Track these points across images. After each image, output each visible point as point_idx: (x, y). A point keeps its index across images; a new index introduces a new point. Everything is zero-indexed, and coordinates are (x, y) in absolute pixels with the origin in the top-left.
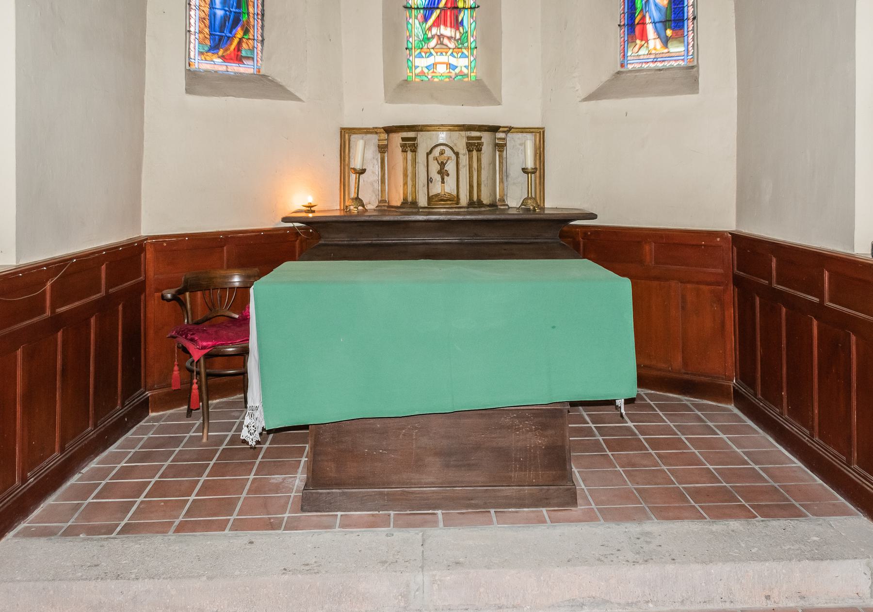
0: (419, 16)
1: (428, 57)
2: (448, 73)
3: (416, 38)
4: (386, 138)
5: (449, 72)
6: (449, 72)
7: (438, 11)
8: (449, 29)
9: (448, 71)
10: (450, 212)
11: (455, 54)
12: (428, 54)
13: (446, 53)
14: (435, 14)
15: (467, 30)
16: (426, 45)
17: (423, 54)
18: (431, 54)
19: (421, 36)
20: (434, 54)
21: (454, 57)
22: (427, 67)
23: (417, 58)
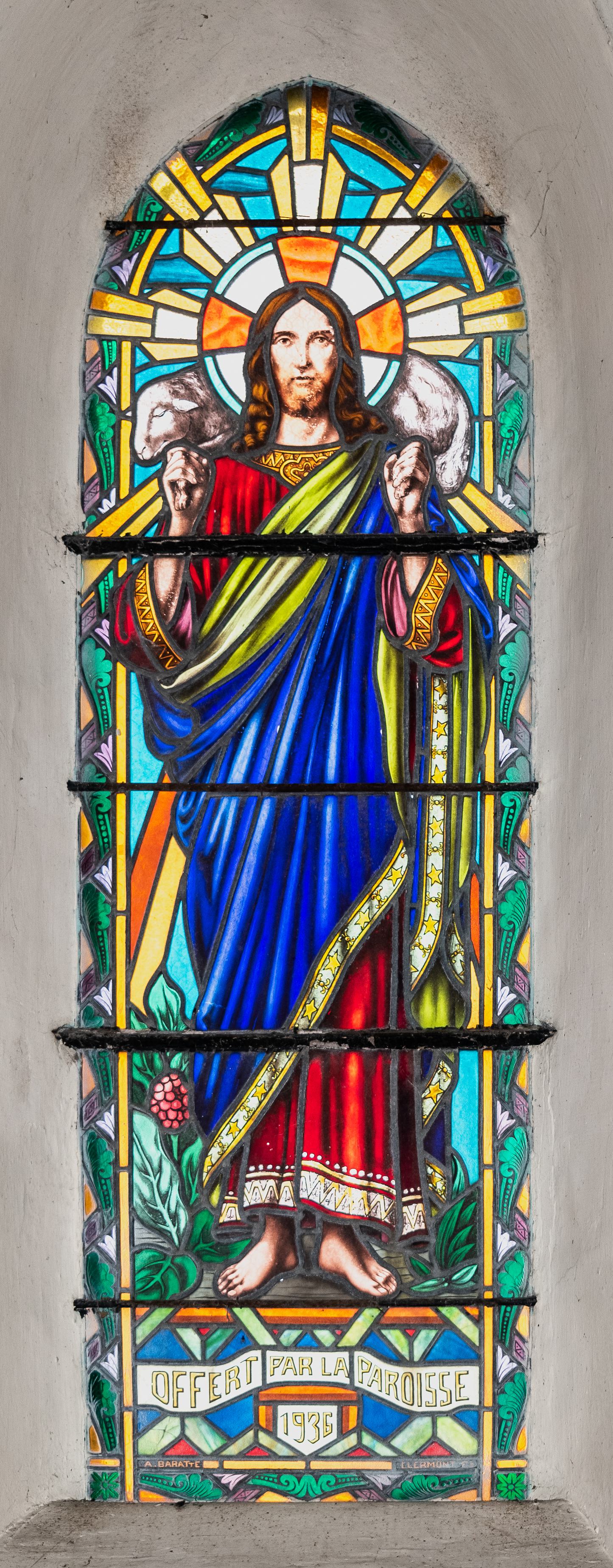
0: (162, 1090)
1: (217, 1360)
2: (346, 1456)
3: (142, 1235)
4: (334, 1409)
5: (359, 1452)
6: (359, 1452)
7: (285, 1060)
8: (354, 1175)
9: (351, 1441)
10: (212, 664)
11: (395, 1337)
12: (219, 1338)
13: (340, 1328)
14: (264, 1077)
15: (473, 1177)
16: (208, 1277)
17: (191, 1338)
18: (245, 1342)
19: (174, 1218)
20: (264, 1337)
21: (396, 1359)
22: (211, 1418)
23: (148, 1362)
